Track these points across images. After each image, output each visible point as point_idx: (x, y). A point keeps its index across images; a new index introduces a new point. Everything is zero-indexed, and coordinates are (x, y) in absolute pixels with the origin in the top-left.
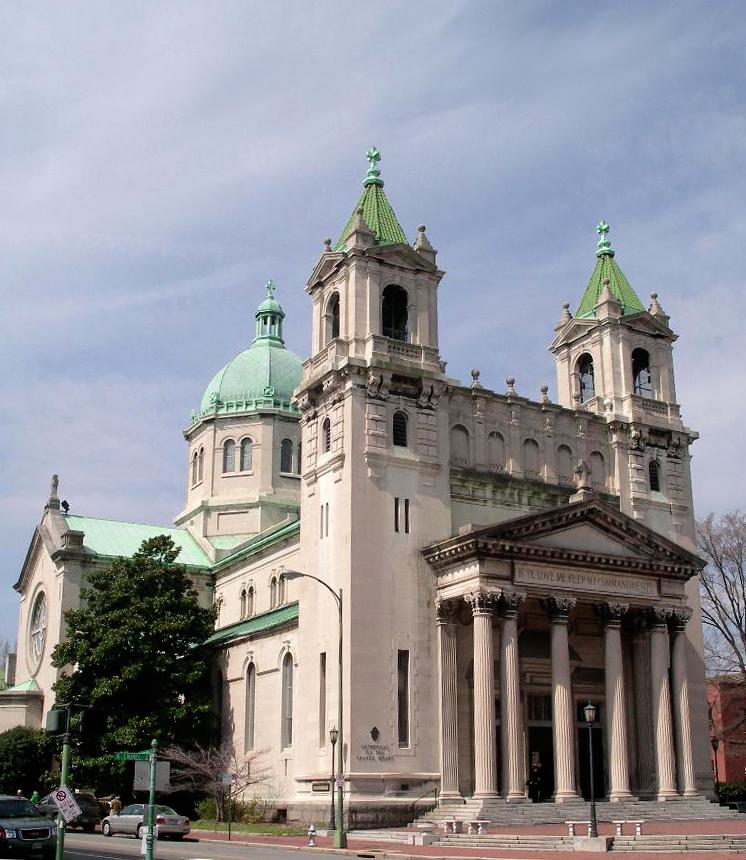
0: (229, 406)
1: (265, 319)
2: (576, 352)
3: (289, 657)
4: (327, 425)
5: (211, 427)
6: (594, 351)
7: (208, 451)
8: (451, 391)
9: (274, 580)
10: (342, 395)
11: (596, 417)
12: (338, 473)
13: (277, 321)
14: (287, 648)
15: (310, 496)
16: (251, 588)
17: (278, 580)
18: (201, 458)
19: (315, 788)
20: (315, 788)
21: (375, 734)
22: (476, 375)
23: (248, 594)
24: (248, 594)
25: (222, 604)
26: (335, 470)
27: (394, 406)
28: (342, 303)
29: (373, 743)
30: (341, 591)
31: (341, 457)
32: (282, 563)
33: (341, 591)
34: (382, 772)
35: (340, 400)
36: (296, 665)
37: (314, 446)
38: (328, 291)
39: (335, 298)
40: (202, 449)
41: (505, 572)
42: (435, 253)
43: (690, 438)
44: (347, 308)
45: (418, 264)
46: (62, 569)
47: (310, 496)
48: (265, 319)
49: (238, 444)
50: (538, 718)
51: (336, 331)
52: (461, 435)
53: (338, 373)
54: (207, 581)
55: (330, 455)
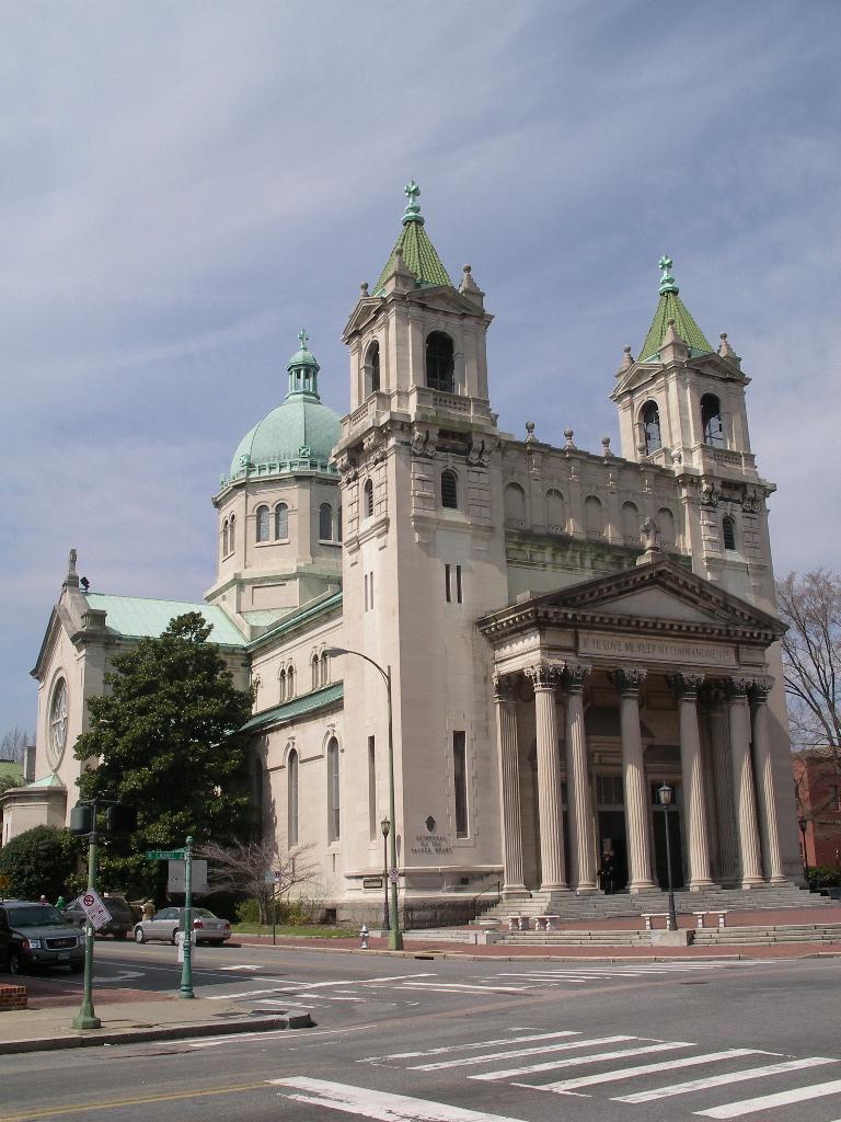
0: (262, 469)
2: (640, 400)
3: (334, 742)
4: (369, 486)
6: (659, 398)
7: (240, 519)
8: (504, 446)
9: (316, 658)
10: (385, 453)
14: (331, 732)
18: (232, 526)
19: (367, 885)
21: (431, 823)
22: (530, 428)
24: (287, 674)
26: (379, 536)
27: (441, 464)
28: (382, 353)
30: (389, 667)
31: (386, 522)
33: (389, 667)
35: (382, 460)
36: (342, 751)
38: (367, 340)
39: (374, 347)
41: (569, 643)
42: (482, 295)
43: (767, 491)
44: (387, 358)
46: (84, 652)
49: (272, 510)
50: (608, 801)
51: (376, 384)
52: (516, 494)
55: (373, 520)
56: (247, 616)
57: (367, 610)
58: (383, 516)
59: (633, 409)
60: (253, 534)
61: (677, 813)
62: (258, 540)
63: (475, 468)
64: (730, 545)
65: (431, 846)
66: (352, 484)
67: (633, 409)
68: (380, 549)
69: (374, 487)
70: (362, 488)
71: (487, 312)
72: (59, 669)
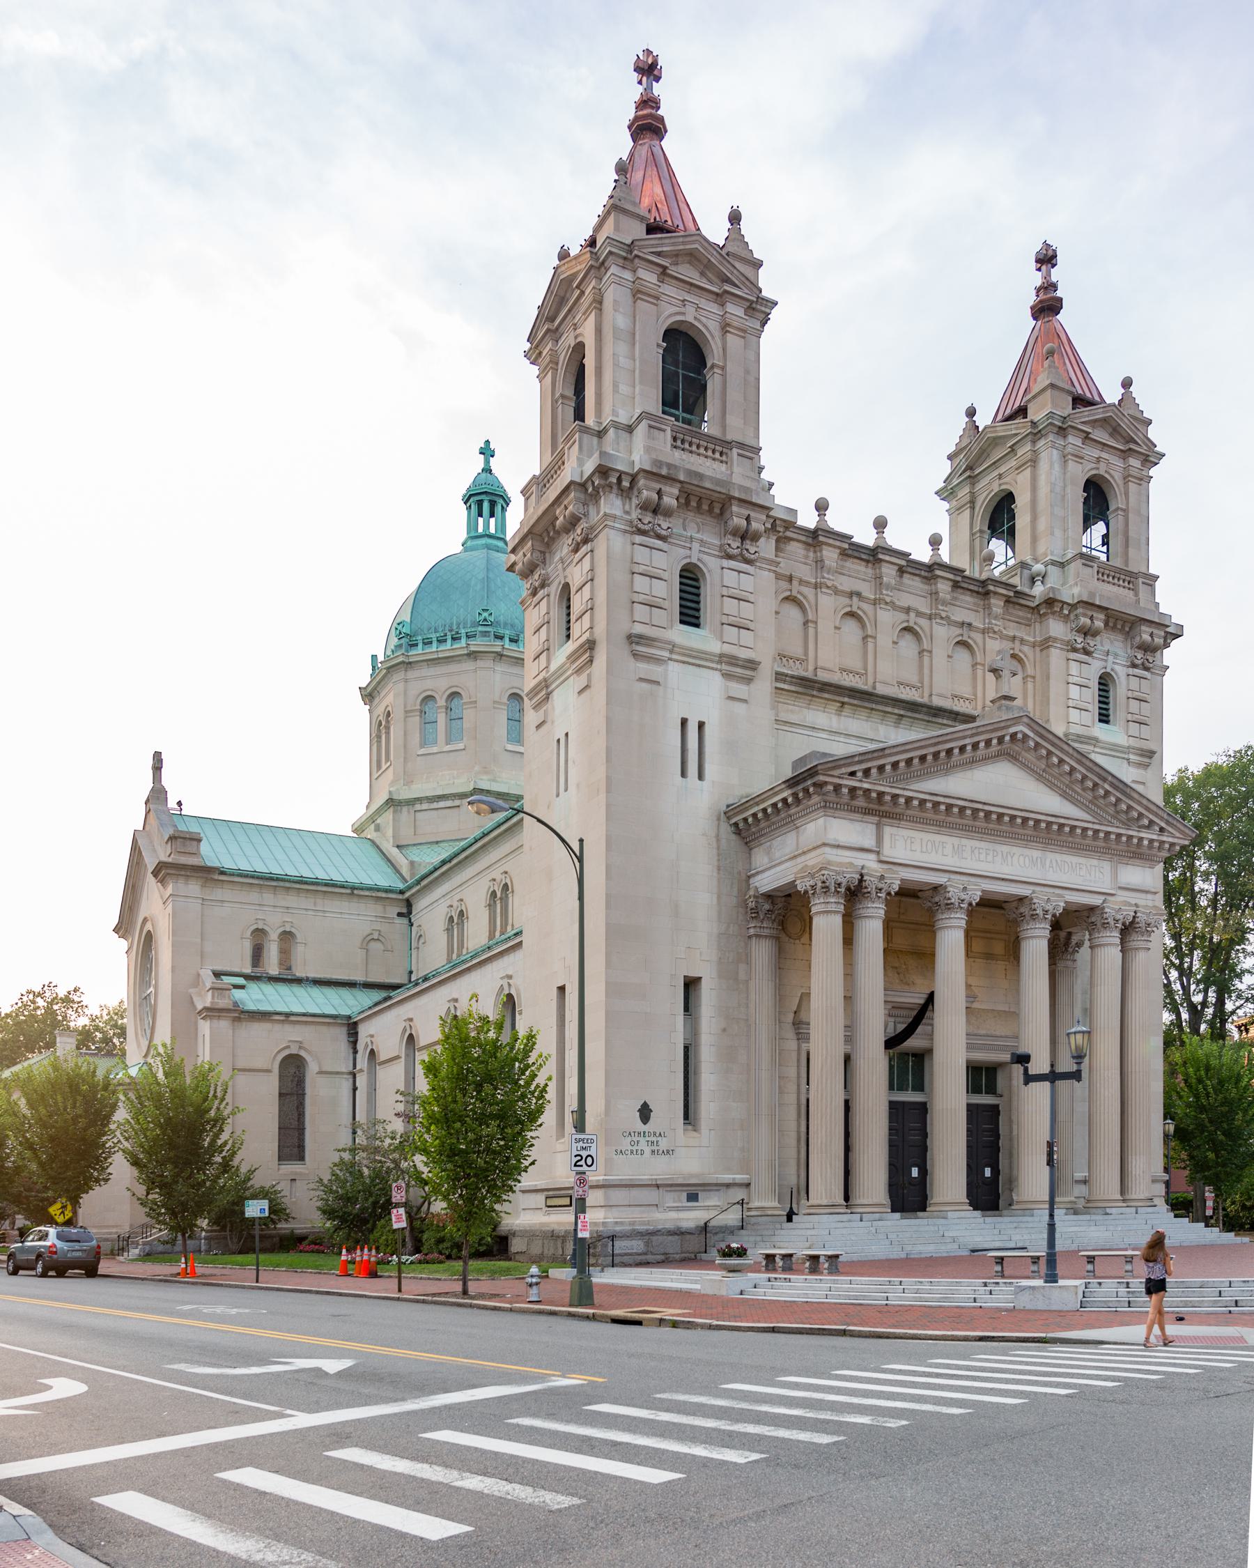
0: (427, 643)
1: (480, 503)
2: (988, 489)
5: (399, 676)
6: (1021, 487)
7: (397, 715)
11: (1019, 594)
12: (584, 676)
13: (498, 509)
14: (506, 987)
15: (538, 727)
16: (462, 911)
17: (499, 895)
18: (387, 728)
19: (550, 1202)
20: (550, 1202)
21: (645, 1113)
23: (457, 921)
24: (457, 921)
25: (422, 940)
26: (578, 671)
27: (683, 552)
29: (640, 1126)
30: (581, 841)
31: (591, 645)
32: (505, 868)
33: (581, 841)
34: (659, 1169)
36: (520, 1014)
37: (544, 611)
39: (580, 348)
40: (389, 714)
41: (869, 842)
43: (1173, 634)
45: (727, 280)
46: (170, 890)
47: (538, 727)
48: (480, 503)
49: (441, 702)
50: (902, 1087)
51: (579, 414)
52: (793, 612)
53: (583, 486)
54: (398, 910)
55: (570, 647)
56: (407, 851)
57: (558, 795)
58: (587, 636)
59: (973, 508)
60: (415, 738)
61: (994, 1110)
62: (423, 744)
63: (733, 564)
64: (1104, 718)
65: (643, 1144)
66: (541, 593)
67: (973, 508)
68: (580, 692)
69: (573, 590)
70: (554, 598)
71: (766, 293)
72: (145, 920)
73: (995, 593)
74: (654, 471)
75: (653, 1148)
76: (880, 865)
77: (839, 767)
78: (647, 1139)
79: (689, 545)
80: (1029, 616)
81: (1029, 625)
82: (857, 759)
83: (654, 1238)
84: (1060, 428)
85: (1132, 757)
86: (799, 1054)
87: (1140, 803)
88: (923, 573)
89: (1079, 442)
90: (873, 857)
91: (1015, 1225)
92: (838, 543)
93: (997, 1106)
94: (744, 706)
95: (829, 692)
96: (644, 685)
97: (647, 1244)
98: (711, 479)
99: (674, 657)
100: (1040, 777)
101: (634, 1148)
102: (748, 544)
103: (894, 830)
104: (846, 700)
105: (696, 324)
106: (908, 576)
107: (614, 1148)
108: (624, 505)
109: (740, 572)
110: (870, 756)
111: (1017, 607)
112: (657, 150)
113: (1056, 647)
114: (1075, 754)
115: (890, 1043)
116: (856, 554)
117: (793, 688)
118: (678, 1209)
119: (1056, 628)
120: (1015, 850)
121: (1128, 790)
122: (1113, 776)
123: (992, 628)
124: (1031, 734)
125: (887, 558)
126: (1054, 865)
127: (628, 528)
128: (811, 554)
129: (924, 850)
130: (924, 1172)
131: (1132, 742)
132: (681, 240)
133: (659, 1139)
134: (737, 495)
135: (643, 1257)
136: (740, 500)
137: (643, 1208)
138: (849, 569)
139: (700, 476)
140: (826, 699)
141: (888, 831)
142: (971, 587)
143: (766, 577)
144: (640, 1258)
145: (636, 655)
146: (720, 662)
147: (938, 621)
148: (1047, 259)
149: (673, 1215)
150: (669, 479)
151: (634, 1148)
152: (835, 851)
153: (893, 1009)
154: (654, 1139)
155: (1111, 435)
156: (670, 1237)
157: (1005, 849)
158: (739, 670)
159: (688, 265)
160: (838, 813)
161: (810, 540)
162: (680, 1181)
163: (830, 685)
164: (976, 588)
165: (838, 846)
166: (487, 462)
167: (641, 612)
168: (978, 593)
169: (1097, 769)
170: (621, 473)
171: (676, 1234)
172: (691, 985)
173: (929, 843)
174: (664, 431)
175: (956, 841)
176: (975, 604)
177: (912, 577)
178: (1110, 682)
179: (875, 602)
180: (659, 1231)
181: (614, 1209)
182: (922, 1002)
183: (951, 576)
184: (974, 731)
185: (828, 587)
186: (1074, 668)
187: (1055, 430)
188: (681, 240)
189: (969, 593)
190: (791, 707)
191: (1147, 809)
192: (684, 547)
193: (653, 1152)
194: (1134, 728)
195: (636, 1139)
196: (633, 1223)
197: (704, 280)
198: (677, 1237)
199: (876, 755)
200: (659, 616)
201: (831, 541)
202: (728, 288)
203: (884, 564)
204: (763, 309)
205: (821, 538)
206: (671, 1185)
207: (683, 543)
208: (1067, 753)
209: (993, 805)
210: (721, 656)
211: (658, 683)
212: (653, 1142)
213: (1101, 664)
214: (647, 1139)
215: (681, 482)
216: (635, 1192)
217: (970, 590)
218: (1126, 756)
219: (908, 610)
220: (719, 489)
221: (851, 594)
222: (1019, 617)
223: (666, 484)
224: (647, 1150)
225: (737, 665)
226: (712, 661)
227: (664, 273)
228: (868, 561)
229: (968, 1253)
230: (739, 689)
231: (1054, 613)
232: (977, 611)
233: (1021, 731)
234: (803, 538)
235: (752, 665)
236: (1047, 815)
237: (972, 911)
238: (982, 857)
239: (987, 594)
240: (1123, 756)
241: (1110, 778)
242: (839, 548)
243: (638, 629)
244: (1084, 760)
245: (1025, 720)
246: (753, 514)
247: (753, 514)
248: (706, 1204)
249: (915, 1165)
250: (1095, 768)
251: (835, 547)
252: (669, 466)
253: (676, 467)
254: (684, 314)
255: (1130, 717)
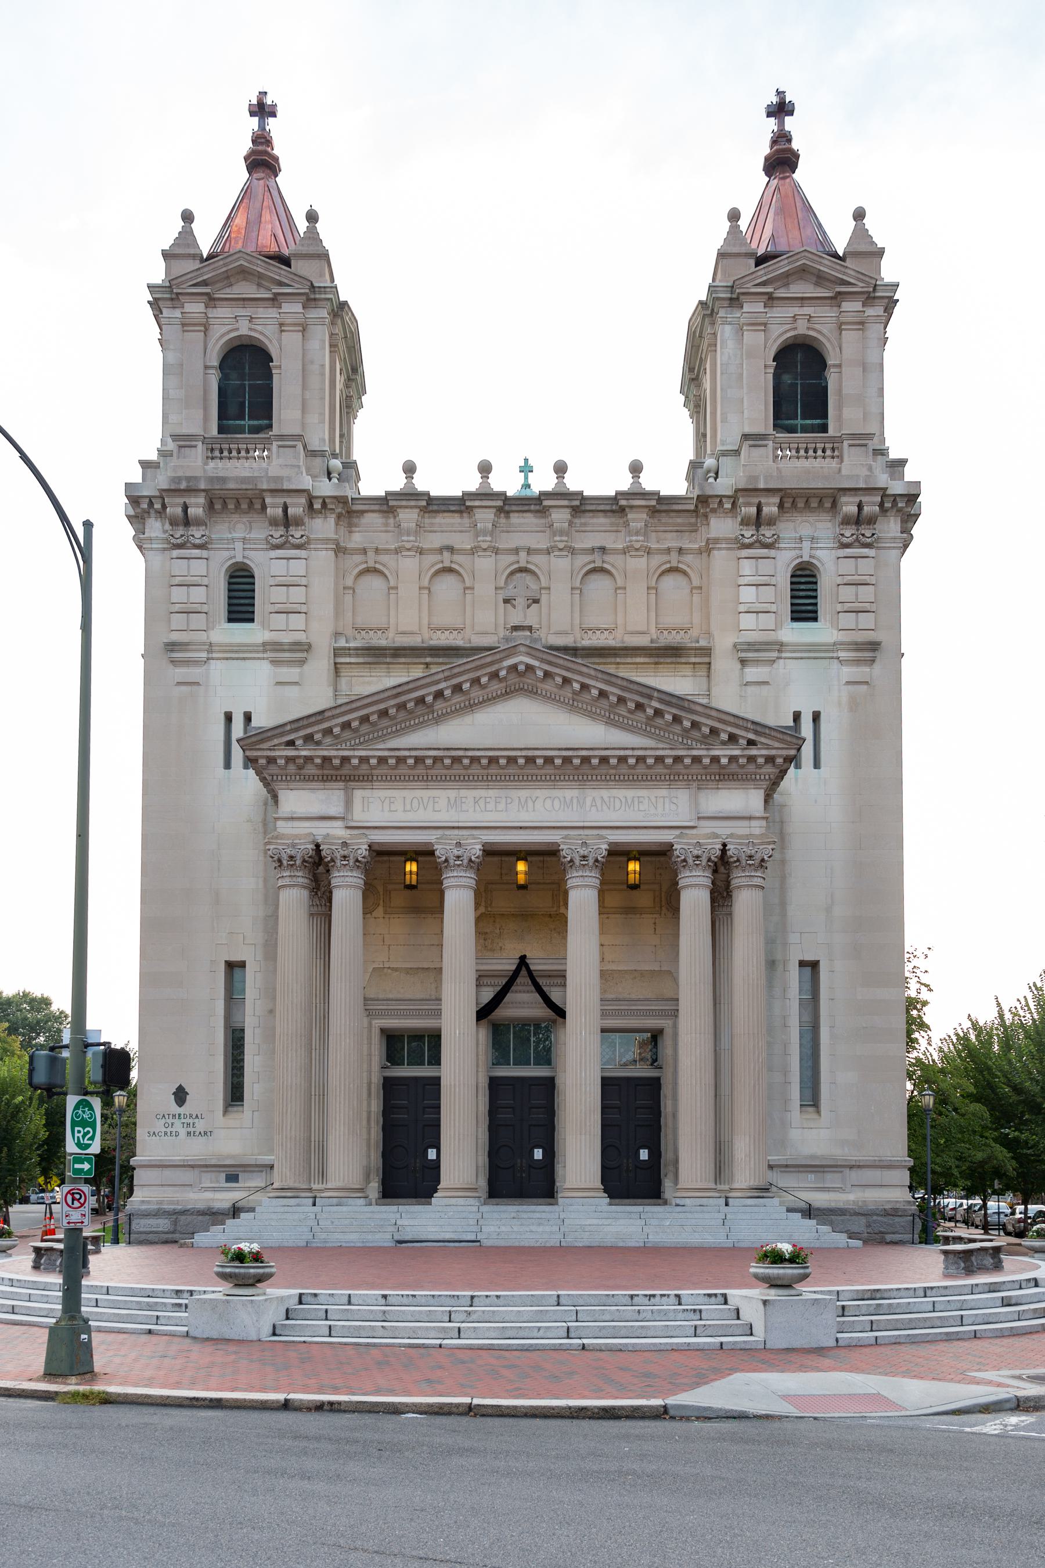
21: (180, 1096)
27: (226, 554)
29: (175, 1109)
34: (195, 1149)
41: (335, 808)
73: (632, 507)
74: (172, 488)
75: (189, 1130)
76: (349, 832)
77: (269, 739)
78: (184, 1121)
79: (232, 546)
80: (693, 520)
81: (696, 531)
82: (288, 728)
83: (183, 1218)
84: (731, 299)
85: (842, 654)
86: (370, 1031)
87: (709, 717)
88: (532, 507)
89: (759, 307)
90: (339, 824)
91: (513, 1215)
92: (413, 503)
93: (658, 1079)
94: (296, 688)
95: (405, 656)
96: (183, 688)
97: (175, 1223)
98: (236, 479)
99: (215, 655)
100: (573, 706)
101: (168, 1130)
102: (292, 530)
103: (367, 793)
104: (428, 660)
105: (253, 334)
106: (516, 515)
107: (147, 1130)
108: (163, 525)
109: (288, 559)
110: (305, 722)
111: (672, 514)
112: (271, 183)
113: (720, 549)
114: (600, 675)
115: (483, 1013)
116: (443, 508)
117: (361, 660)
118: (214, 1189)
119: (722, 526)
120: (538, 793)
121: (686, 704)
122: (659, 691)
123: (632, 546)
124: (536, 663)
125: (477, 503)
126: (599, 803)
127: (166, 546)
128: (391, 521)
129: (408, 807)
130: (550, 1154)
131: (842, 637)
132: (221, 263)
133: (196, 1120)
134: (265, 487)
135: (170, 1236)
136: (272, 491)
137: (177, 1188)
138: (440, 524)
139: (224, 480)
140: (404, 663)
141: (358, 794)
142: (602, 507)
143: (323, 558)
144: (167, 1236)
145: (174, 662)
146: (264, 651)
147: (556, 553)
148: (781, 109)
149: (209, 1195)
150: (190, 491)
151: (168, 1130)
152: (290, 824)
153: (481, 979)
154: (191, 1121)
155: (817, 284)
156: (200, 1218)
157: (523, 794)
158: (287, 655)
159: (244, 283)
160: (292, 785)
161: (385, 508)
162: (213, 1162)
163: (404, 649)
164: (608, 508)
165: (292, 819)
166: (526, 478)
167: (178, 621)
168: (612, 511)
169: (635, 687)
170: (150, 498)
171: (206, 1214)
172: (234, 967)
173: (415, 801)
174: (195, 446)
175: (452, 794)
176: (612, 524)
177: (521, 514)
178: (816, 572)
179: (473, 551)
180: (188, 1210)
181: (145, 1189)
182: (514, 967)
183: (565, 503)
184: (446, 674)
185: (409, 550)
186: (747, 567)
187: (726, 303)
188: (221, 263)
189: (601, 514)
190: (367, 679)
191: (720, 721)
192: (228, 549)
193: (189, 1133)
194: (848, 620)
195: (170, 1121)
196: (161, 1203)
197: (262, 290)
198: (208, 1217)
199: (313, 719)
200: (199, 621)
201: (404, 503)
202: (277, 290)
203: (476, 510)
204: (323, 296)
205: (391, 503)
206: (206, 1166)
207: (226, 546)
208: (589, 676)
209: (479, 749)
210: (264, 644)
211: (198, 684)
212: (188, 1124)
213: (793, 553)
214: (184, 1121)
215: (203, 490)
216: (167, 1172)
217: (601, 511)
218: (835, 655)
219: (516, 551)
220: (244, 487)
221: (441, 550)
222: (679, 525)
223: (190, 497)
224: (183, 1132)
225: (284, 651)
226: (258, 652)
227: (211, 301)
228: (461, 512)
229: (393, 1244)
230: (290, 673)
231: (713, 511)
232: (617, 531)
233: (521, 662)
234: (376, 507)
235: (304, 649)
236: (559, 749)
237: (477, 867)
238: (490, 807)
239: (622, 510)
240: (831, 655)
241: (656, 694)
242: (416, 507)
243: (175, 637)
244: (613, 680)
245: (522, 649)
246: (289, 501)
247: (289, 501)
248: (247, 1185)
249: (538, 1147)
250: (631, 686)
251: (411, 507)
252: (189, 479)
253: (195, 478)
254: (237, 329)
255: (839, 607)
